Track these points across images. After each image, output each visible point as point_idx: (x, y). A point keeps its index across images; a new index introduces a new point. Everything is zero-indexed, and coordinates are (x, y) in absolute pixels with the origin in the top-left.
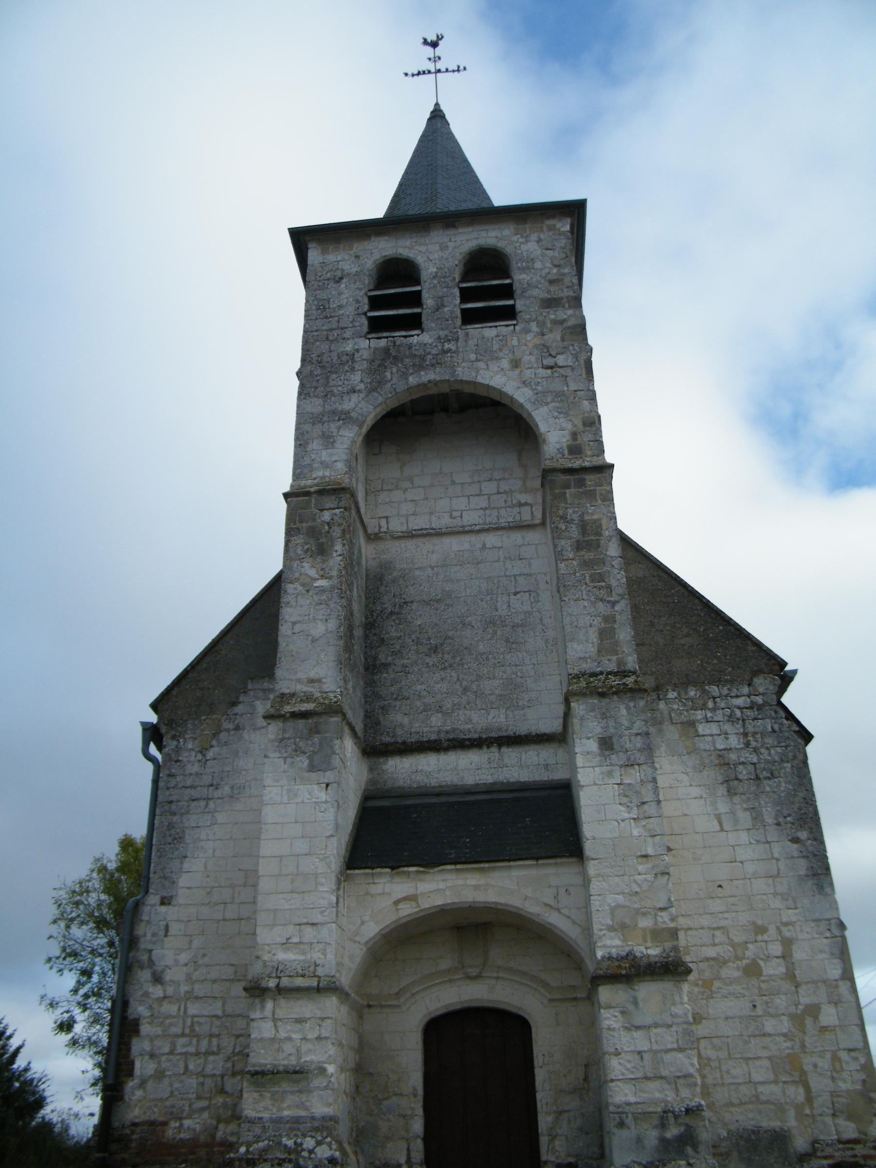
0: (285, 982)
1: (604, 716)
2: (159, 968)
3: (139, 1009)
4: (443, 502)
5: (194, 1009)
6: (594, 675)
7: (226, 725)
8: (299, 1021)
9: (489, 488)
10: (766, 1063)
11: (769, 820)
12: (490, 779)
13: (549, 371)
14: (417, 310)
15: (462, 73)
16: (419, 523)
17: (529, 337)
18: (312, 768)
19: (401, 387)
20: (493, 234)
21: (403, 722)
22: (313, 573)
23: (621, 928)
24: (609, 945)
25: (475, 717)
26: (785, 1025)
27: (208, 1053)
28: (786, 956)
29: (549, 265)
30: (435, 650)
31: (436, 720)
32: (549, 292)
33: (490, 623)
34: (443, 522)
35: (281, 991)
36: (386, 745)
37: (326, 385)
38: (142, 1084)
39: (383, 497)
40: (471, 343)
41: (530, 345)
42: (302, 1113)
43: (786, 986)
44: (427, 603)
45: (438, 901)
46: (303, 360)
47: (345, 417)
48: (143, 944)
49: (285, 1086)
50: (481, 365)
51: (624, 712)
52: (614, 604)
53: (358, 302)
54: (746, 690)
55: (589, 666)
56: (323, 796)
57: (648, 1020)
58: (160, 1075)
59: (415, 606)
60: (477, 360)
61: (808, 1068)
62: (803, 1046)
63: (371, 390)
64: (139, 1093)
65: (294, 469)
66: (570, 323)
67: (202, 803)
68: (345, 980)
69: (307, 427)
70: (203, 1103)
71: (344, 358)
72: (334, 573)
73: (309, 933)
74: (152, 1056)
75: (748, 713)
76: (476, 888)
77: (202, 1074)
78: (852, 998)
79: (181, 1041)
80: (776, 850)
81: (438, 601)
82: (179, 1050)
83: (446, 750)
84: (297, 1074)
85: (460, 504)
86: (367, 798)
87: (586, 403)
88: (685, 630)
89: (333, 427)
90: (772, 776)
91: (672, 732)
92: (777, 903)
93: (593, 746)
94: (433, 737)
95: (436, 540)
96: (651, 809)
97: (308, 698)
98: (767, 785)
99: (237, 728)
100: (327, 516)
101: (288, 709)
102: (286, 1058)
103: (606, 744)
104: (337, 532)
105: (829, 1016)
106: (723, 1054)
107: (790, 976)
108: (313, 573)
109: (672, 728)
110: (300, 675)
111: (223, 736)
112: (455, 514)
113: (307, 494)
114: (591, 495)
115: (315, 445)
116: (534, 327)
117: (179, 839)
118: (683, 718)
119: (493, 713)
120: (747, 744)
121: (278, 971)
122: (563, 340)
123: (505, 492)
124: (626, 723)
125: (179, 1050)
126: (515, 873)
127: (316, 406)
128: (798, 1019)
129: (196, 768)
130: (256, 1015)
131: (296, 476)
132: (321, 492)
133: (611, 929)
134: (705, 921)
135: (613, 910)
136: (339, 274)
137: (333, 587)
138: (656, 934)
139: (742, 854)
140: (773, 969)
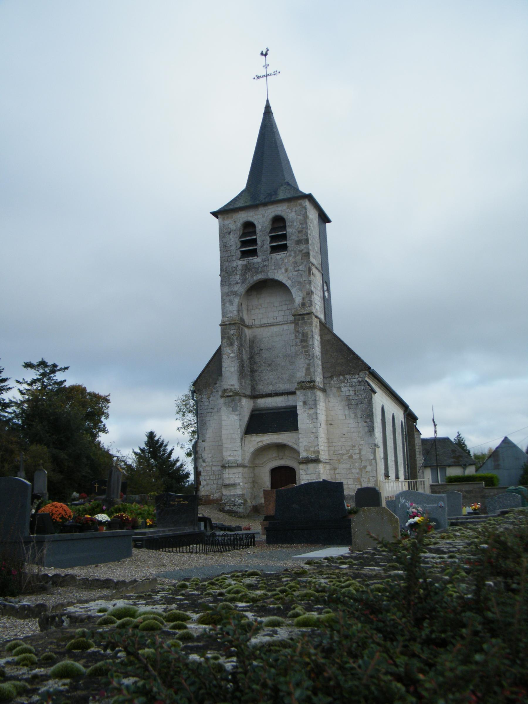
0: (230, 465)
1: (305, 395)
2: (204, 458)
3: (200, 469)
4: (269, 318)
5: (214, 468)
6: (304, 382)
7: (214, 390)
8: (234, 473)
9: (285, 308)
10: (352, 480)
11: (359, 416)
12: (285, 405)
13: (297, 272)
14: (256, 247)
15: (278, 75)
16: (264, 321)
17: (291, 258)
18: (233, 411)
19: (252, 282)
20: (280, 209)
21: (262, 388)
22: (230, 351)
23: (306, 450)
24: (303, 455)
25: (281, 386)
26: (358, 471)
27: (218, 479)
28: (360, 453)
29: (298, 224)
30: (270, 365)
31: (271, 387)
32: (298, 237)
33: (285, 356)
34: (271, 321)
35: (229, 467)
36: (257, 395)
37: (229, 281)
38: (204, 487)
39: (253, 311)
40: (273, 262)
41: (291, 262)
42: (235, 493)
43: (360, 461)
44: (267, 350)
45: (268, 442)
46: (221, 270)
47: (235, 293)
48: (199, 453)
49: (231, 488)
50: (276, 271)
51: (310, 394)
52: (310, 360)
53: (236, 244)
54: (357, 376)
55: (303, 379)
56: (236, 418)
57: (310, 473)
58: (207, 485)
59: (264, 351)
60: (275, 269)
61: (362, 481)
62: (361, 476)
63: (243, 283)
64: (203, 489)
65: (222, 313)
66: (304, 252)
67: (210, 414)
68: (246, 463)
69: (224, 297)
70: (218, 491)
71: (234, 269)
72: (235, 352)
73: (235, 453)
74: (205, 480)
75: (357, 384)
76: (276, 439)
77: (217, 484)
78: (375, 464)
79: (211, 476)
80: (360, 425)
81: (270, 349)
82: (211, 478)
83: (273, 396)
84: (234, 485)
85: (276, 314)
86: (253, 411)
87: (308, 285)
88: (341, 357)
89: (232, 297)
90: (361, 403)
91: (334, 390)
92: (359, 439)
93: (301, 403)
94: (270, 392)
95: (269, 328)
96: (315, 420)
97: (231, 391)
98: (359, 406)
99: (217, 391)
100: (232, 332)
101: (226, 394)
102: (231, 482)
103: (305, 403)
104: (235, 338)
105: (369, 468)
106: (341, 478)
107: (360, 458)
108: (230, 351)
109: (334, 389)
110: (229, 383)
111: (213, 394)
112: (275, 318)
113: (226, 325)
114: (306, 323)
115: (227, 305)
116: (292, 253)
117: (205, 424)
118: (338, 386)
119: (286, 385)
120: (355, 394)
121: (228, 462)
122: (302, 259)
123: (290, 309)
124: (310, 397)
125: (211, 478)
126: (286, 435)
127: (226, 289)
128: (361, 469)
129: (207, 404)
130: (224, 472)
131: (223, 316)
132: (230, 324)
133: (304, 451)
134: (340, 444)
135: (304, 446)
136: (229, 230)
137: (235, 357)
138: (314, 452)
139: (351, 426)
140: (356, 457)
